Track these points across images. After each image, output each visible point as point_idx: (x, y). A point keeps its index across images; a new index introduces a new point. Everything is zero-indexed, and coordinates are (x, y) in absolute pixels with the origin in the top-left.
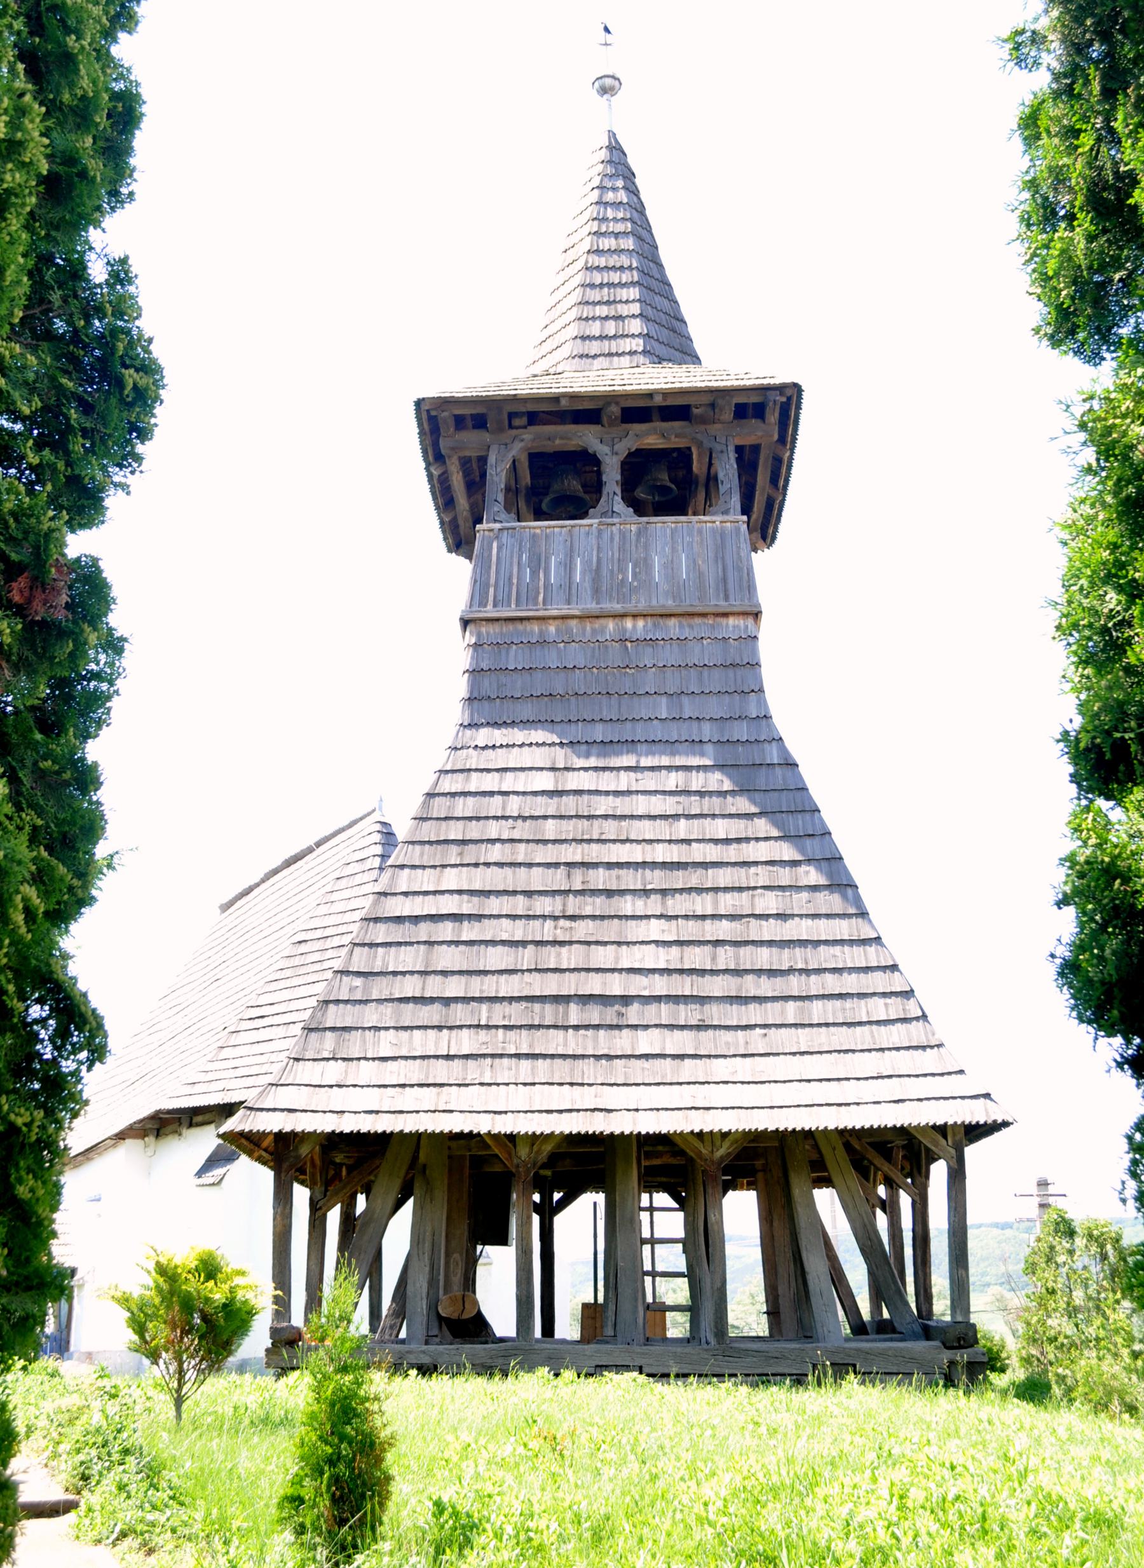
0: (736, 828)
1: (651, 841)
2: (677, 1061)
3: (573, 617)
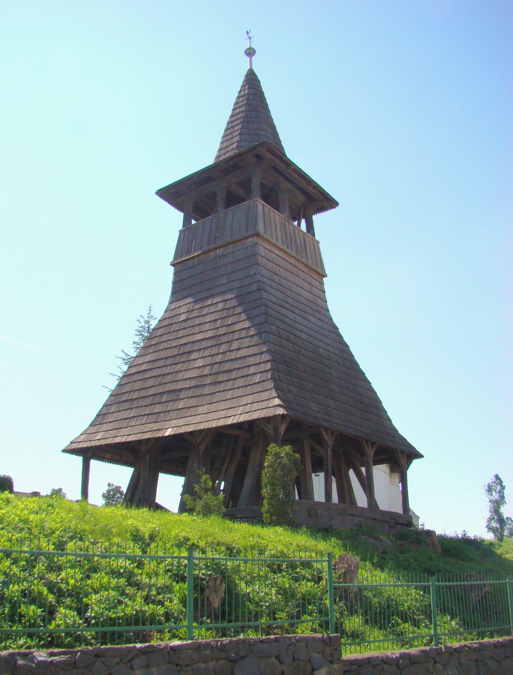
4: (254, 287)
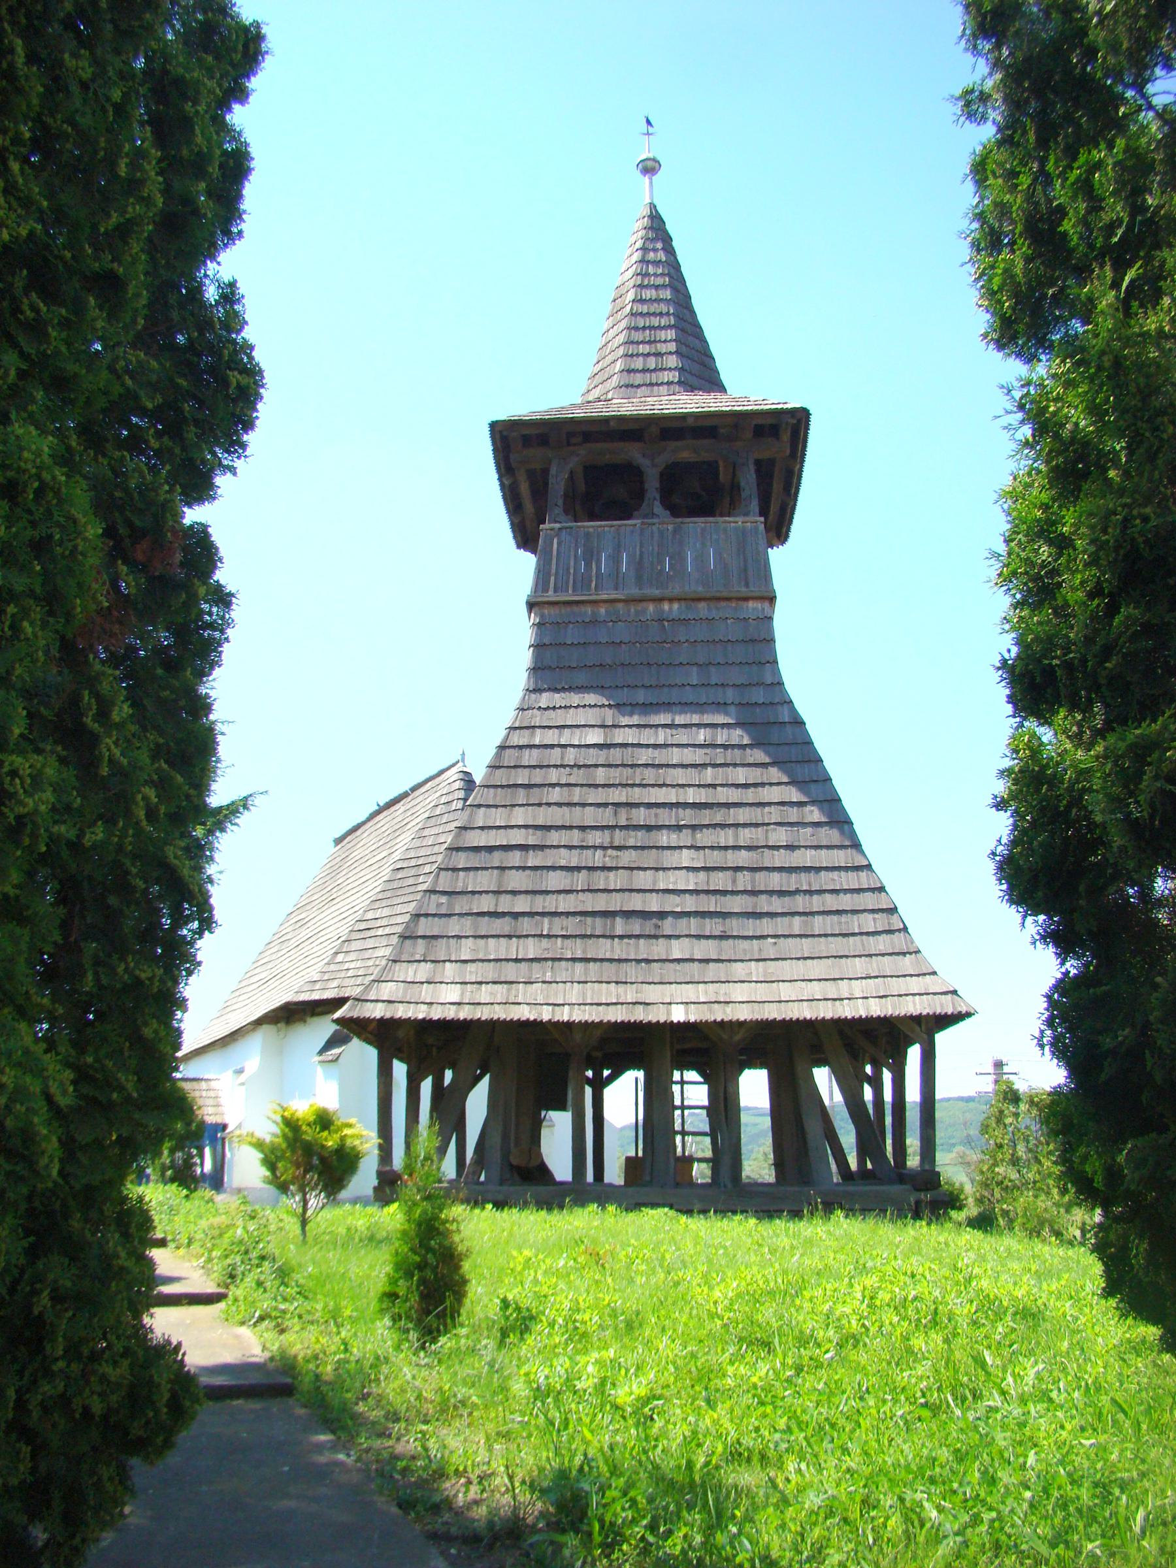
0: (754, 775)
2: (703, 964)
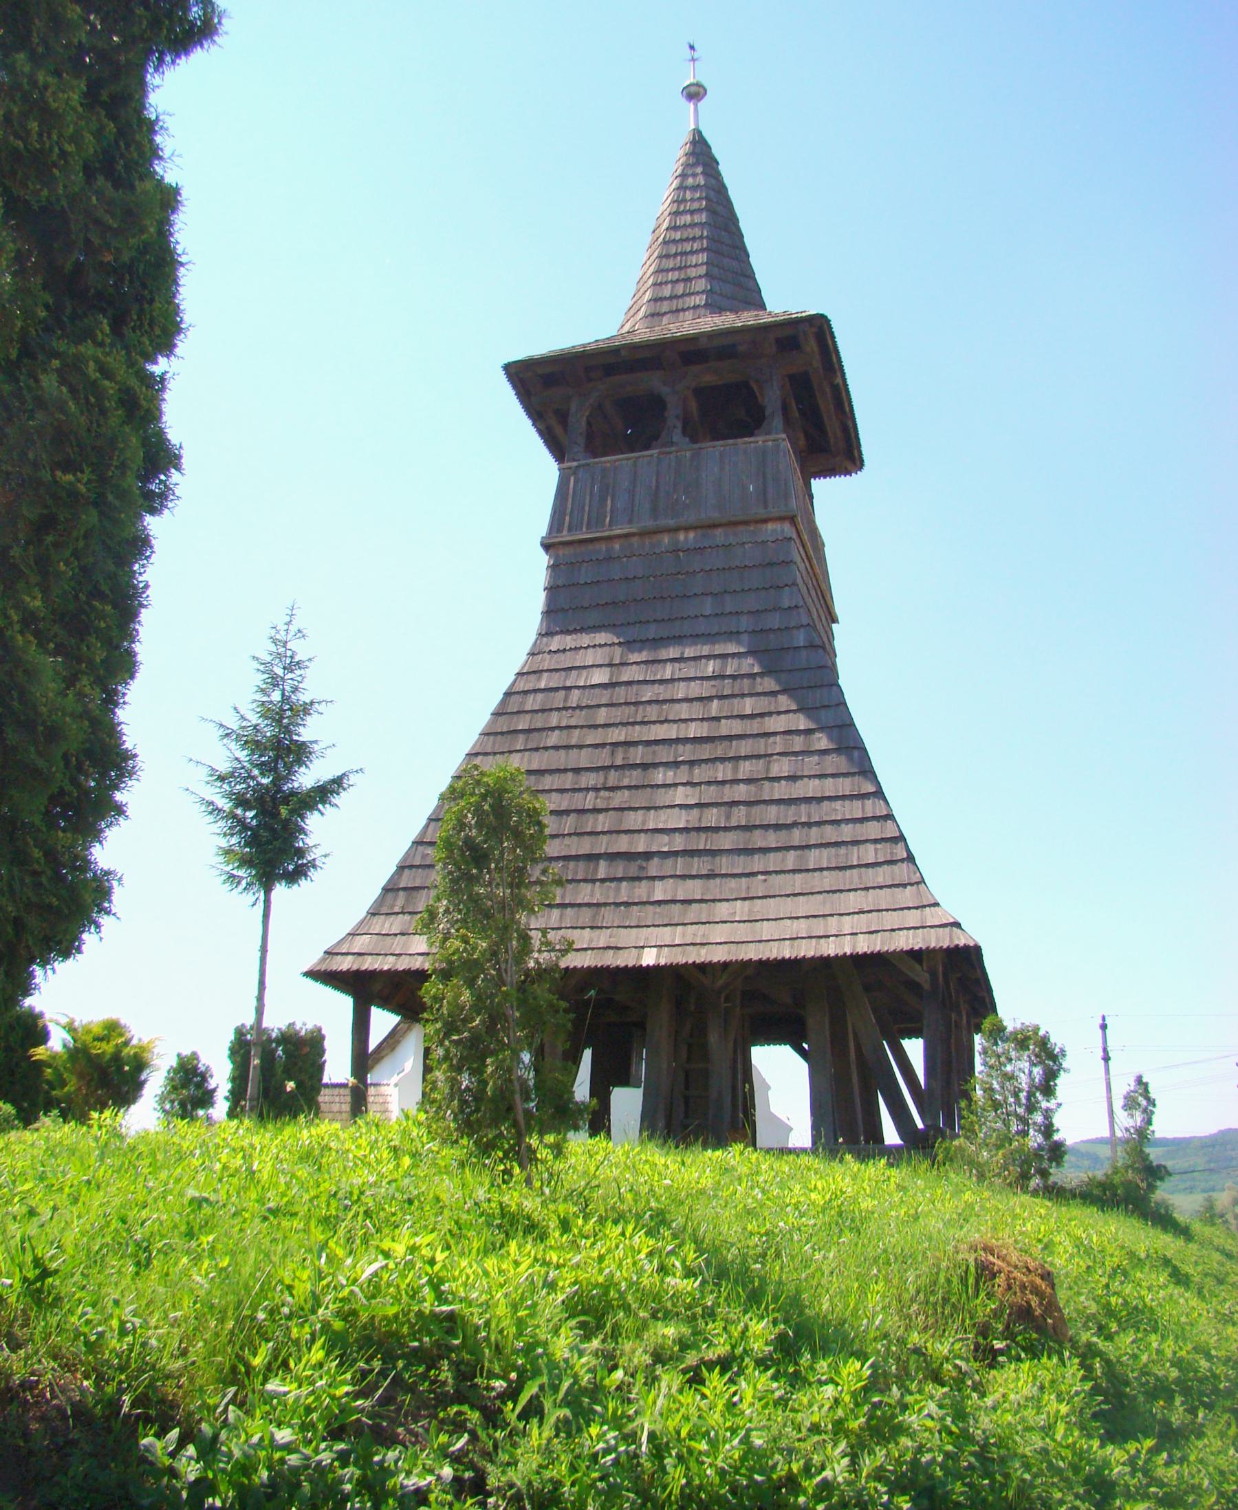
0: (762, 704)
1: (685, 721)
3: (633, 535)
4: (800, 639)
